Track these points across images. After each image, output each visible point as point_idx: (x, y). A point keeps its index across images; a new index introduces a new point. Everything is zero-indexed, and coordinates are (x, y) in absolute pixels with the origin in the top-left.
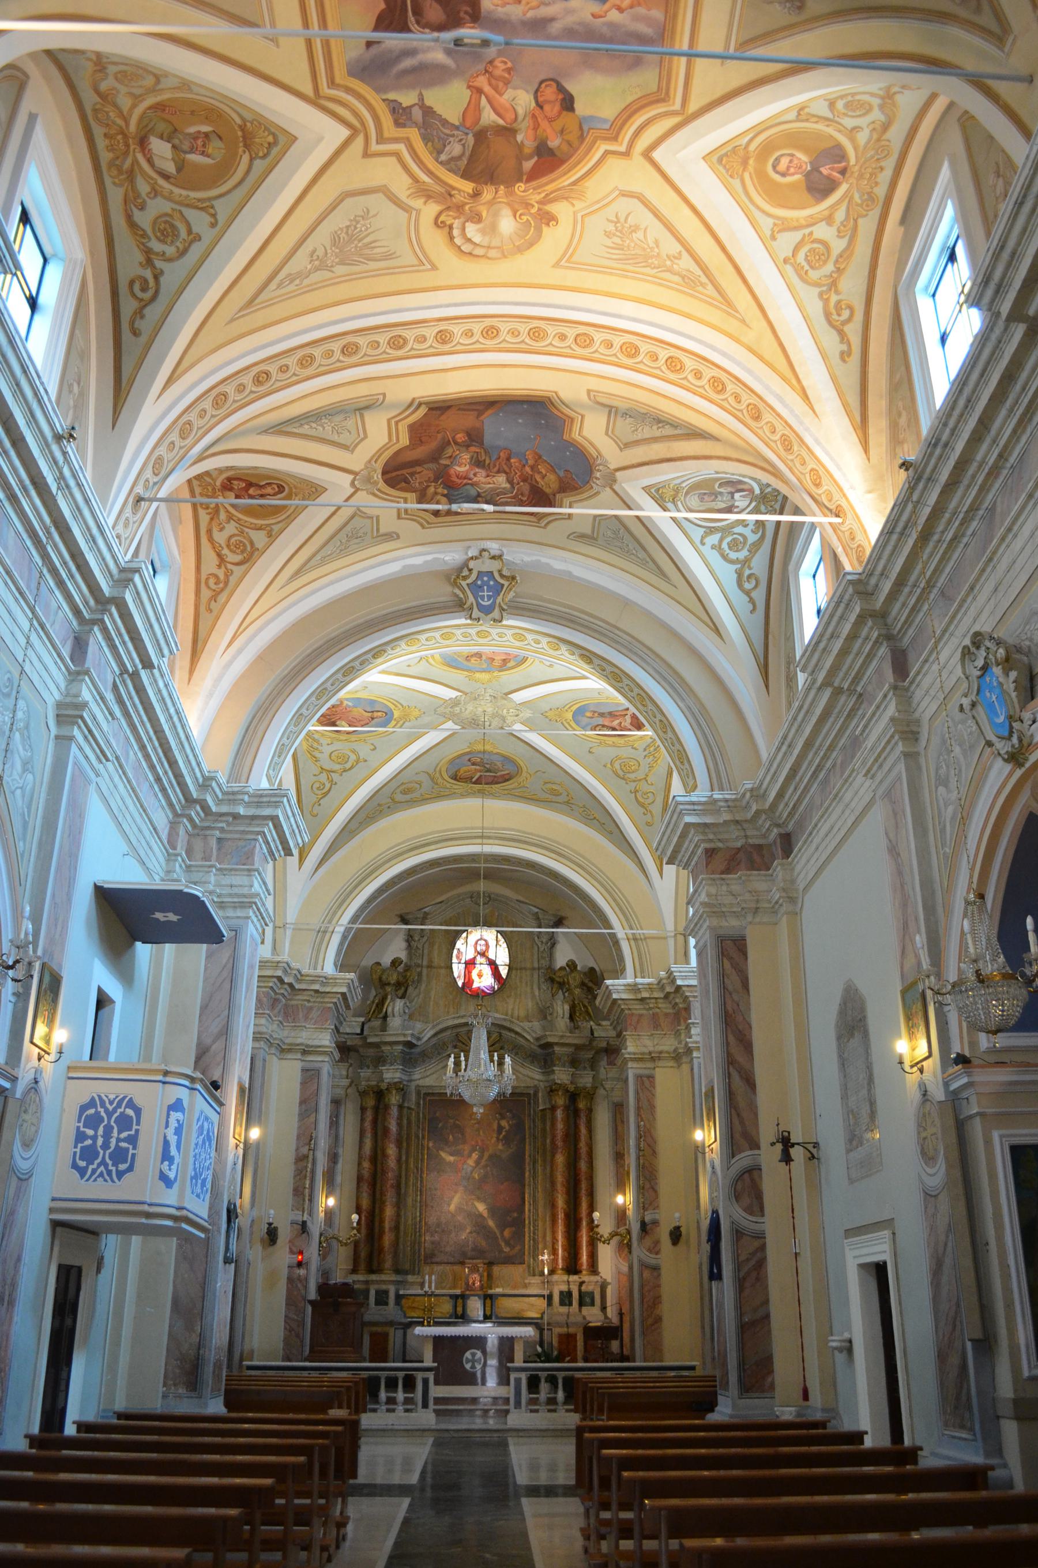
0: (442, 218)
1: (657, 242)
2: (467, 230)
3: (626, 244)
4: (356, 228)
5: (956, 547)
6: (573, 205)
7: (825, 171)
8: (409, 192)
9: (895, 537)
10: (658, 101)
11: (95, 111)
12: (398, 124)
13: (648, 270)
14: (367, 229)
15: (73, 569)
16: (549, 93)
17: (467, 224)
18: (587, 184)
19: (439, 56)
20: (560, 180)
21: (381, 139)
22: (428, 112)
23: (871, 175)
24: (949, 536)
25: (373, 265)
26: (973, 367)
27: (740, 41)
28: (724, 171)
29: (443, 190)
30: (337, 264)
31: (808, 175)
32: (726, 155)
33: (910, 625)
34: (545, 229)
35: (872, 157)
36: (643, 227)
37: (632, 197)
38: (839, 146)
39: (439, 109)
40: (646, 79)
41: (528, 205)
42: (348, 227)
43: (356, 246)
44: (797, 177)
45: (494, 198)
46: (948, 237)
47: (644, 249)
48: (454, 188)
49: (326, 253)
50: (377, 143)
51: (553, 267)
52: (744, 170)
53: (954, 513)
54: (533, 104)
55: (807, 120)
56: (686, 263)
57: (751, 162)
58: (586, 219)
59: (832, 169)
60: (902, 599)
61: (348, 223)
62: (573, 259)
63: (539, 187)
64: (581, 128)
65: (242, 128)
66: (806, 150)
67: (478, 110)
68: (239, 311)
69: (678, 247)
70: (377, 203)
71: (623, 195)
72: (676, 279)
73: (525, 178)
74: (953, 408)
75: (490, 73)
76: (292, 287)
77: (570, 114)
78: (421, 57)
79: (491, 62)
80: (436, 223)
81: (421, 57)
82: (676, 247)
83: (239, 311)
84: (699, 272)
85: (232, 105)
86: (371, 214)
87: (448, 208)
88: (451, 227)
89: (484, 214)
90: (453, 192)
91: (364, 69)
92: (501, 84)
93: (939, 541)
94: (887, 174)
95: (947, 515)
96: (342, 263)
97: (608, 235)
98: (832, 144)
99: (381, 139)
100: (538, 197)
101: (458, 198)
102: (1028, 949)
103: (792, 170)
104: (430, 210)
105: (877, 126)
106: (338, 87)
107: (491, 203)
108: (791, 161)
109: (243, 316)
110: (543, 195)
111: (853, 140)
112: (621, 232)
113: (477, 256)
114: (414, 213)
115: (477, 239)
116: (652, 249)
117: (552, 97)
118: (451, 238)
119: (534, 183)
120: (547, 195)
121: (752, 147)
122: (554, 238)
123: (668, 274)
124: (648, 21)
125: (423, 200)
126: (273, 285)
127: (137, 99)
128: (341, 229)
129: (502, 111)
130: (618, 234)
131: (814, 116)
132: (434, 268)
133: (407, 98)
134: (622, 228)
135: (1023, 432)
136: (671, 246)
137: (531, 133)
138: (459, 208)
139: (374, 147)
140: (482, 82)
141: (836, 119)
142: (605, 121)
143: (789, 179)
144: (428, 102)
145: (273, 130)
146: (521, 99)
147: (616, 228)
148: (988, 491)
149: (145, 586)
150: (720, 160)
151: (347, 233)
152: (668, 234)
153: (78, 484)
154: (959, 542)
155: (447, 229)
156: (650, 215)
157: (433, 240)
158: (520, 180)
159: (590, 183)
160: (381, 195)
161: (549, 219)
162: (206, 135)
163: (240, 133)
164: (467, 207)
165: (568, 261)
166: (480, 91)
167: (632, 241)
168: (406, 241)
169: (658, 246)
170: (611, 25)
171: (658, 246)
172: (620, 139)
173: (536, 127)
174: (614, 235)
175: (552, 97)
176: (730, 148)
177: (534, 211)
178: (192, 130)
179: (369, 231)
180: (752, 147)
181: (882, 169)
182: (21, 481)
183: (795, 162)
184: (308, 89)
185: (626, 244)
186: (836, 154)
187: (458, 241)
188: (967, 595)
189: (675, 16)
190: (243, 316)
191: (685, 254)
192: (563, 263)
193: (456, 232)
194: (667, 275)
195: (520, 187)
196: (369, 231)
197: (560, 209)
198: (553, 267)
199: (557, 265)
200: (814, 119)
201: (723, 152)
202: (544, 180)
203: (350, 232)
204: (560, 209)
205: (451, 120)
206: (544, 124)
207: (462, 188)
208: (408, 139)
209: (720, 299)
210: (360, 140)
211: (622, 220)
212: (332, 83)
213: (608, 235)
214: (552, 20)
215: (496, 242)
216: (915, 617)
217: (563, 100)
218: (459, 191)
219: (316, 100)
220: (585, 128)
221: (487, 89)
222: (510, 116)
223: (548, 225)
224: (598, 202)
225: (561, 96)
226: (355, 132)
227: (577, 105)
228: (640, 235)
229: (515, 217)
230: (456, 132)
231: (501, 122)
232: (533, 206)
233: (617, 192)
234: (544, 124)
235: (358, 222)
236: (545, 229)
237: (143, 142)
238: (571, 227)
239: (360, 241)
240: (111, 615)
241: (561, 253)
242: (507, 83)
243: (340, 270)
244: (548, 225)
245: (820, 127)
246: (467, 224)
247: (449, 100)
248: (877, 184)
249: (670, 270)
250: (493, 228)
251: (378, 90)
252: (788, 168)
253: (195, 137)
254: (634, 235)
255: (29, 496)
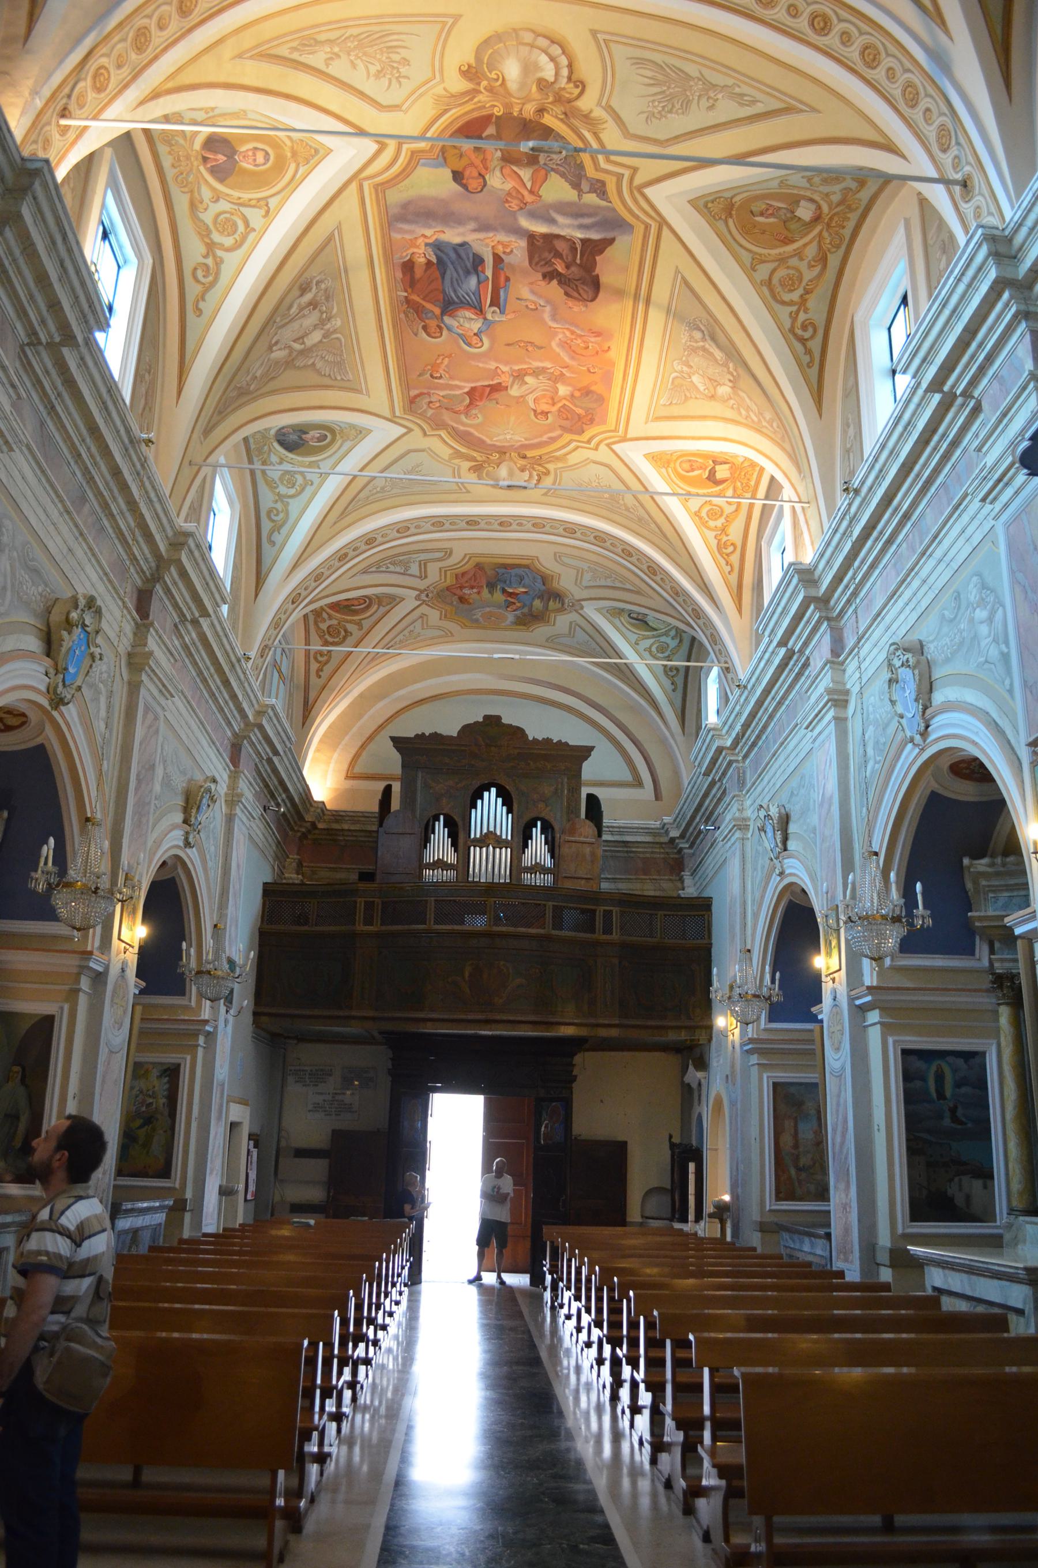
0: (577, 91)
1: (354, 66)
2: (553, 72)
3: (385, 55)
4: (663, 107)
5: (71, 453)
6: (445, 89)
7: (221, 158)
8: (604, 126)
9: (103, 390)
10: (383, 184)
11: (838, 247)
12: (603, 184)
13: (355, 31)
14: (654, 101)
15: (936, 438)
16: (474, 184)
17: (552, 79)
18: (434, 112)
19: (560, 219)
20: (462, 112)
21: (620, 177)
22: (576, 186)
23: (179, 160)
24: (83, 451)
25: (658, 58)
26: (164, 509)
27: (332, 242)
28: (310, 143)
29: (572, 120)
30: (694, 79)
31: (234, 152)
32: (313, 156)
33: (24, 366)
34: (472, 62)
35: (188, 174)
36: (372, 79)
37: (389, 107)
38: (221, 181)
39: (567, 186)
40: (395, 196)
41: (490, 90)
42: (670, 112)
43: (669, 88)
44: (243, 149)
45: (524, 104)
46: (117, 241)
47: (365, 54)
48: (561, 120)
49: (700, 96)
50: (623, 175)
51: (461, 16)
52: (293, 148)
53: (114, 499)
54: (487, 177)
55: (259, 200)
56: (317, 60)
57: (289, 155)
58: (430, 75)
59: (216, 160)
60: (53, 372)
61: (669, 115)
62: (438, 27)
63: (480, 108)
64: (445, 159)
65: (731, 216)
66: (244, 171)
67: (533, 179)
68: (802, 111)
69: (331, 70)
70: (637, 126)
71: (397, 106)
72: (322, 37)
73: (494, 120)
74: (153, 487)
75: (522, 202)
76: (745, 89)
77: (455, 169)
78: (576, 222)
79: (521, 209)
80: (584, 87)
81: (576, 222)
82: (334, 70)
83: (802, 111)
84: (302, 59)
85: (729, 237)
86: (645, 115)
87: (569, 101)
88: (569, 79)
89: (534, 88)
90: (562, 117)
91: (621, 226)
92: (514, 194)
93: (83, 440)
94: (167, 162)
95: (98, 458)
96: (688, 77)
97: (406, 62)
98: (226, 182)
99: (620, 177)
100: (480, 97)
101: (558, 110)
102: (181, 959)
103: (250, 153)
104: (587, 103)
105: (201, 207)
106: (644, 222)
107: (527, 100)
108: (255, 160)
109: (801, 102)
110: (476, 100)
111: (213, 189)
112: (393, 68)
113: (545, 37)
114: (604, 103)
115: (544, 59)
116: (357, 57)
117: (470, 181)
118: (570, 66)
119: (484, 113)
120: (471, 99)
121: (293, 166)
122: (461, 51)
123: (332, 38)
124: (401, 231)
125: (593, 115)
126: (759, 108)
127: (799, 254)
128: (677, 113)
129: (514, 175)
130: (395, 65)
131: (254, 206)
132: (594, 33)
133: (591, 199)
134: (392, 70)
135: (115, 532)
136: (338, 69)
137: (488, 156)
138: (558, 99)
139: (627, 173)
140: (529, 198)
141: (236, 207)
142: (424, 165)
143: (250, 146)
144: (575, 193)
145: (705, 210)
146: (496, 181)
147: (398, 71)
148: (95, 496)
149: (914, 355)
150: (317, 151)
151: (673, 106)
152: (345, 79)
153: (876, 460)
154: (73, 457)
155: (574, 78)
156: (368, 92)
157: (590, 68)
158: (497, 117)
159: (431, 113)
160: (632, 131)
161: (469, 73)
162: (762, 214)
163: (734, 212)
164: (551, 99)
165: (444, 23)
166: (531, 192)
167: (379, 60)
168: (617, 76)
169: (352, 62)
170: (430, 227)
171: (352, 62)
172: (409, 153)
173: (484, 161)
174: (399, 62)
175: (470, 181)
176: (312, 162)
177: (484, 83)
178: (772, 220)
179: (652, 98)
180: (293, 166)
181: (173, 166)
182: (892, 515)
183: (250, 161)
184: (666, 231)
185: (385, 55)
186: (221, 173)
187: (564, 61)
188: (64, 506)
189: (383, 237)
190: (801, 102)
191: (323, 67)
192: (451, 21)
193: (565, 72)
194: (332, 35)
195: (498, 111)
196: (652, 98)
197: (458, 85)
198: (461, 16)
199: (457, 18)
200: (253, 203)
201: (316, 158)
202: (476, 114)
203: (670, 106)
204: (458, 85)
205: (558, 176)
206: (478, 162)
207: (553, 119)
208: (596, 170)
209: (272, 52)
210: (637, 181)
211: (394, 81)
212: (647, 227)
213: (406, 62)
214: (475, 230)
215: (525, 50)
216: (31, 380)
217: (463, 179)
218: (556, 117)
219: (663, 223)
220: (441, 159)
221: (526, 193)
222: (506, 171)
223: (469, 66)
224: (421, 95)
225: (464, 181)
226: (640, 189)
227: (451, 175)
228: (373, 69)
229: (504, 79)
230: (555, 167)
231: (515, 168)
232: (485, 88)
233: (404, 108)
234: (478, 162)
235: (659, 112)
236: (472, 62)
237: (817, 219)
238: (445, 64)
239: (664, 92)
240: (953, 386)
241: (453, 33)
242: (509, 194)
243: (692, 70)
244: (469, 66)
245: (246, 196)
246: (552, 79)
247: (557, 189)
248: (170, 153)
249: (330, 42)
250: (528, 68)
251: (614, 210)
252: (254, 155)
253: (772, 215)
254: (379, 68)
255: (899, 504)
